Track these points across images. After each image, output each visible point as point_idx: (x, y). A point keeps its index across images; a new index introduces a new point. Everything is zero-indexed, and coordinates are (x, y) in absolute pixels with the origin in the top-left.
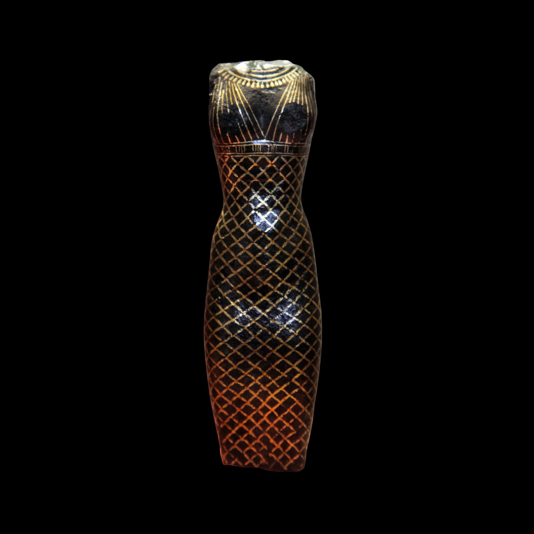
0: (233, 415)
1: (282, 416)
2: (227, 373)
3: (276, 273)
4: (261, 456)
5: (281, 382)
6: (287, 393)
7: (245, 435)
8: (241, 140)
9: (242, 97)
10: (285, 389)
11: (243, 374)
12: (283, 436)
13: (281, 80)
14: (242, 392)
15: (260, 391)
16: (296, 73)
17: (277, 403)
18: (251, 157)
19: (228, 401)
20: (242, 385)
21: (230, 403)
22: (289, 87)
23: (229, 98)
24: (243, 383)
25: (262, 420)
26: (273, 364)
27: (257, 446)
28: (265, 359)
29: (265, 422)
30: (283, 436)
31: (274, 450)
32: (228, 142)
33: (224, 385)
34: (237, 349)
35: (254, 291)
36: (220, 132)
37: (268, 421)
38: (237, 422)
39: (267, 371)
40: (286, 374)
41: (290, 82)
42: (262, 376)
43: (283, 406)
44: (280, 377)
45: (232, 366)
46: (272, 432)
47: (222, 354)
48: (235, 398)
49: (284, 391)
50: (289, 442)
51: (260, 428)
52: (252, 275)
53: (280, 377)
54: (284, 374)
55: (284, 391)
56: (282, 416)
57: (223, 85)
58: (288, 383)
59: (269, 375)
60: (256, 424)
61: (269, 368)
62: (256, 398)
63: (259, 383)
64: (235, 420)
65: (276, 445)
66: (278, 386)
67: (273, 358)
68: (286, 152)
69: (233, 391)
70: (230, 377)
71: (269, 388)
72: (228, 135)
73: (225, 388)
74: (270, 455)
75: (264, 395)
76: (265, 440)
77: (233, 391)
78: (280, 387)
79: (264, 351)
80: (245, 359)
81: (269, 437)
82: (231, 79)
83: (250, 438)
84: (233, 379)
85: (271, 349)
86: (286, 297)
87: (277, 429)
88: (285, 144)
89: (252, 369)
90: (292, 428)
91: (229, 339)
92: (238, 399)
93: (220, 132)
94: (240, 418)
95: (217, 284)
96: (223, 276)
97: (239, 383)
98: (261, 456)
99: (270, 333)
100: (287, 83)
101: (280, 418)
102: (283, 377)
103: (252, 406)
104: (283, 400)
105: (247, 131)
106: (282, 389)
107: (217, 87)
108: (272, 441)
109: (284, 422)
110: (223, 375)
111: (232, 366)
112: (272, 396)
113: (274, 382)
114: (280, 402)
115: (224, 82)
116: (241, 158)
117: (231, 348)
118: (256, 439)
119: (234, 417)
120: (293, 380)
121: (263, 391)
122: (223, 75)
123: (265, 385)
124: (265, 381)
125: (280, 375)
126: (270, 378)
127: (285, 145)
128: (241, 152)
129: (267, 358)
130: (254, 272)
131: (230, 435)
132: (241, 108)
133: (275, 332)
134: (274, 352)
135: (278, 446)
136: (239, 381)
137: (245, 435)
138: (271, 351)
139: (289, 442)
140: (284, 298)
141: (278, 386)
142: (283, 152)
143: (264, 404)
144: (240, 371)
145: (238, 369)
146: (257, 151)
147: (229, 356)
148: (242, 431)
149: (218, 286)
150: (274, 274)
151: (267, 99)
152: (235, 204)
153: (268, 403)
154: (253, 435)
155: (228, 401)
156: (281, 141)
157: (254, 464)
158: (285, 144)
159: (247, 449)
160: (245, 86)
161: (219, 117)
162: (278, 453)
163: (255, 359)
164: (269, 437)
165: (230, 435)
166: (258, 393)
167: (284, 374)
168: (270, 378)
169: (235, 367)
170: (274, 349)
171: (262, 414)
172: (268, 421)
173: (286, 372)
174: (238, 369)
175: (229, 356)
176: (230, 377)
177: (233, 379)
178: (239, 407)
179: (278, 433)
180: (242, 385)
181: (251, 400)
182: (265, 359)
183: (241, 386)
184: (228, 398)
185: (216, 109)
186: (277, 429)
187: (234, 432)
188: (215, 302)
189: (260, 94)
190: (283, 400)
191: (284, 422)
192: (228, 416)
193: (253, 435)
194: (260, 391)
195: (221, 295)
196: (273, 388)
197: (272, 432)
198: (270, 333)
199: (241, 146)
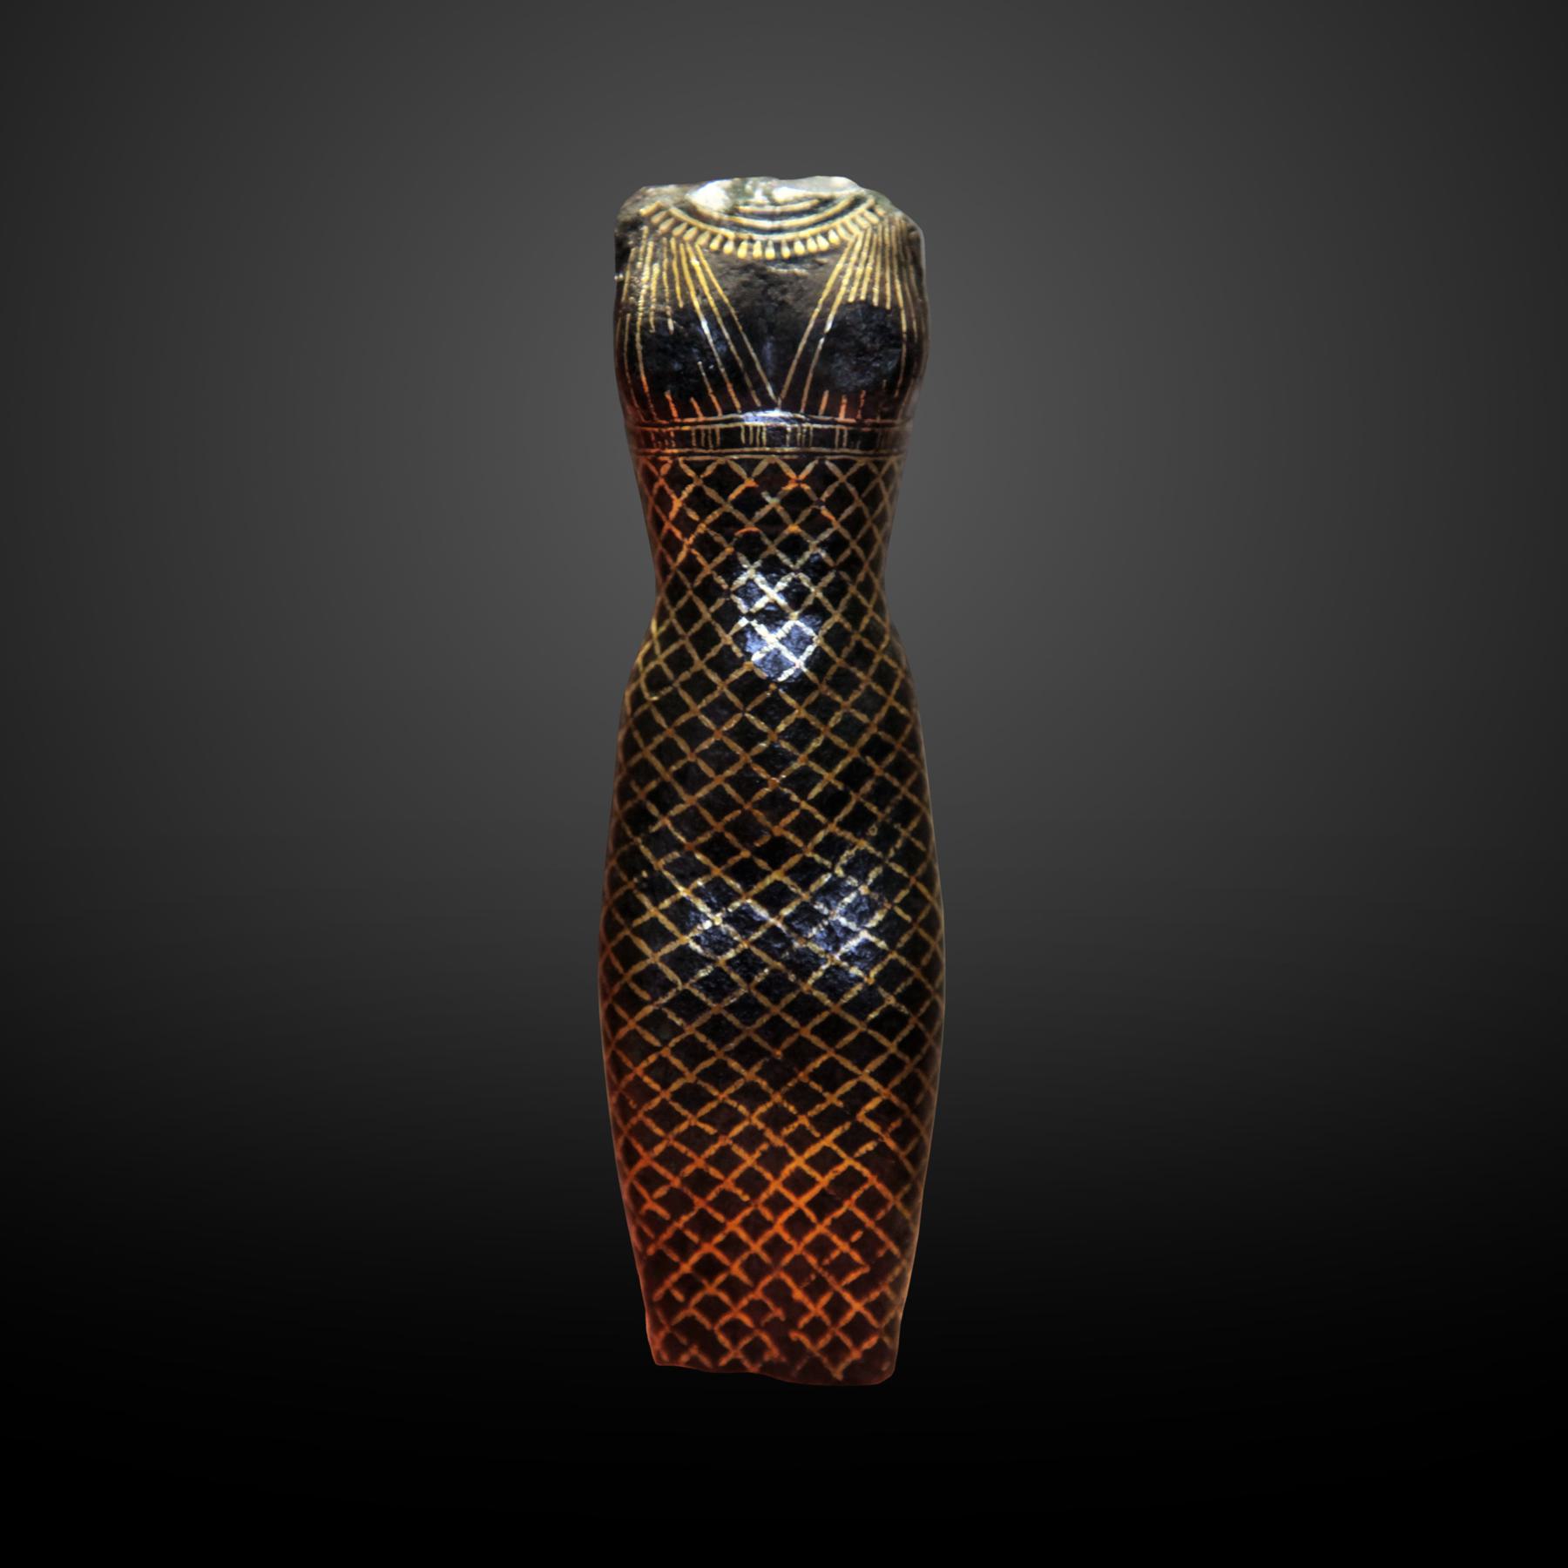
0: (685, 1218)
1: (828, 1221)
2: (666, 1095)
3: (811, 803)
4: (765, 1338)
5: (826, 1122)
6: (842, 1154)
7: (721, 1278)
8: (709, 410)
9: (710, 284)
10: (836, 1141)
11: (712, 1098)
12: (831, 1279)
13: (825, 234)
14: (712, 1151)
15: (764, 1147)
16: (868, 214)
17: (813, 1182)
18: (738, 462)
19: (669, 1176)
20: (710, 1130)
21: (676, 1183)
22: (849, 256)
23: (672, 287)
24: (713, 1124)
25: (769, 1234)
26: (802, 1068)
27: (756, 1309)
28: (779, 1053)
29: (777, 1238)
30: (831, 1279)
31: (804, 1321)
32: (668, 416)
33: (659, 1132)
34: (695, 1025)
35: (745, 854)
36: (646, 389)
37: (786, 1237)
38: (695, 1238)
39: (784, 1089)
40: (841, 1098)
41: (851, 240)
42: (769, 1105)
43: (832, 1193)
44: (821, 1107)
45: (680, 1074)
46: (798, 1269)
47: (651, 1039)
48: (689, 1170)
49: (835, 1147)
50: (847, 1297)
51: (765, 1257)
52: (740, 807)
53: (821, 1107)
54: (833, 1099)
55: (835, 1147)
56: (828, 1221)
57: (655, 250)
58: (847, 1126)
59: (789, 1102)
60: (751, 1244)
61: (789, 1079)
62: (750, 1169)
63: (761, 1126)
64: (689, 1234)
65: (810, 1306)
66: (817, 1135)
67: (803, 1053)
68: (840, 446)
69: (683, 1149)
70: (677, 1106)
71: (789, 1139)
72: (668, 396)
73: (660, 1139)
74: (794, 1335)
75: (775, 1159)
76: (779, 1292)
77: (683, 1149)
78: (822, 1137)
79: (776, 1030)
80: (720, 1055)
81: (790, 1282)
82: (677, 231)
83: (733, 1287)
84: (684, 1112)
85: (795, 1024)
86: (840, 872)
87: (812, 1260)
88: (836, 423)
89: (740, 1084)
90: (856, 1257)
91: (671, 995)
92: (698, 1171)
93: (646, 389)
94: (706, 1226)
95: (636, 833)
96: (654, 811)
97: (701, 1125)
98: (765, 1338)
99: (792, 977)
100: (843, 243)
101: (821, 1229)
102: (832, 1107)
103: (739, 1192)
104: (831, 1176)
105: (725, 385)
106: (828, 1141)
107: (637, 254)
108: (798, 1295)
109: (835, 1239)
110: (656, 1101)
111: (680, 1074)
112: (799, 1162)
113: (803, 1120)
114: (823, 1181)
115: (657, 241)
116: (709, 463)
117: (679, 1022)
118: (752, 1289)
119: (686, 1225)
120: (861, 1116)
121: (773, 1148)
122: (656, 219)
123: (777, 1132)
124: (777, 1119)
125: (823, 1100)
126: (792, 1109)
127: (838, 427)
128: (707, 447)
129: (784, 1052)
130: (747, 798)
131: (674, 1277)
132: (707, 318)
133: (808, 975)
134: (806, 1032)
135: (817, 1309)
136: (702, 1119)
137: (721, 1278)
138: (795, 1030)
139: (847, 1297)
140: (835, 875)
141: (817, 1135)
142: (832, 446)
143: (776, 1186)
144: (704, 1090)
145: (700, 1082)
146: (754, 445)
147: (672, 1044)
148: (709, 1267)
149: (639, 840)
150: (804, 805)
151: (784, 292)
152: (690, 599)
153: (786, 1184)
154: (744, 1278)
155: (669, 1176)
156: (826, 414)
157: (746, 1363)
158: (836, 423)
159: (726, 1318)
161: (643, 342)
162: (815, 1329)
163: (748, 1054)
164: (790, 1282)
165: (674, 1277)
166: (757, 1155)
167: (833, 1099)
168: (792, 1109)
169: (690, 1077)
170: (804, 1024)
171: (768, 1215)
172: (786, 1237)
173: (840, 1091)
174: (700, 1082)
175: (672, 1044)
176: (677, 1106)
177: (684, 1112)
178: (703, 1196)
179: (815, 1271)
180: (710, 1130)
181: (736, 1174)
182: (779, 1053)
183: (707, 1135)
184: (668, 1168)
185: (634, 320)
186: (812, 1260)
187: (686, 1268)
188: (631, 885)
189: (764, 277)
190: (831, 1176)
191: (835, 1239)
192: (670, 1223)
193: (744, 1278)
194: (764, 1147)
195: (649, 867)
196: (801, 1141)
197: (798, 1269)
198: (792, 977)
199: (709, 427)
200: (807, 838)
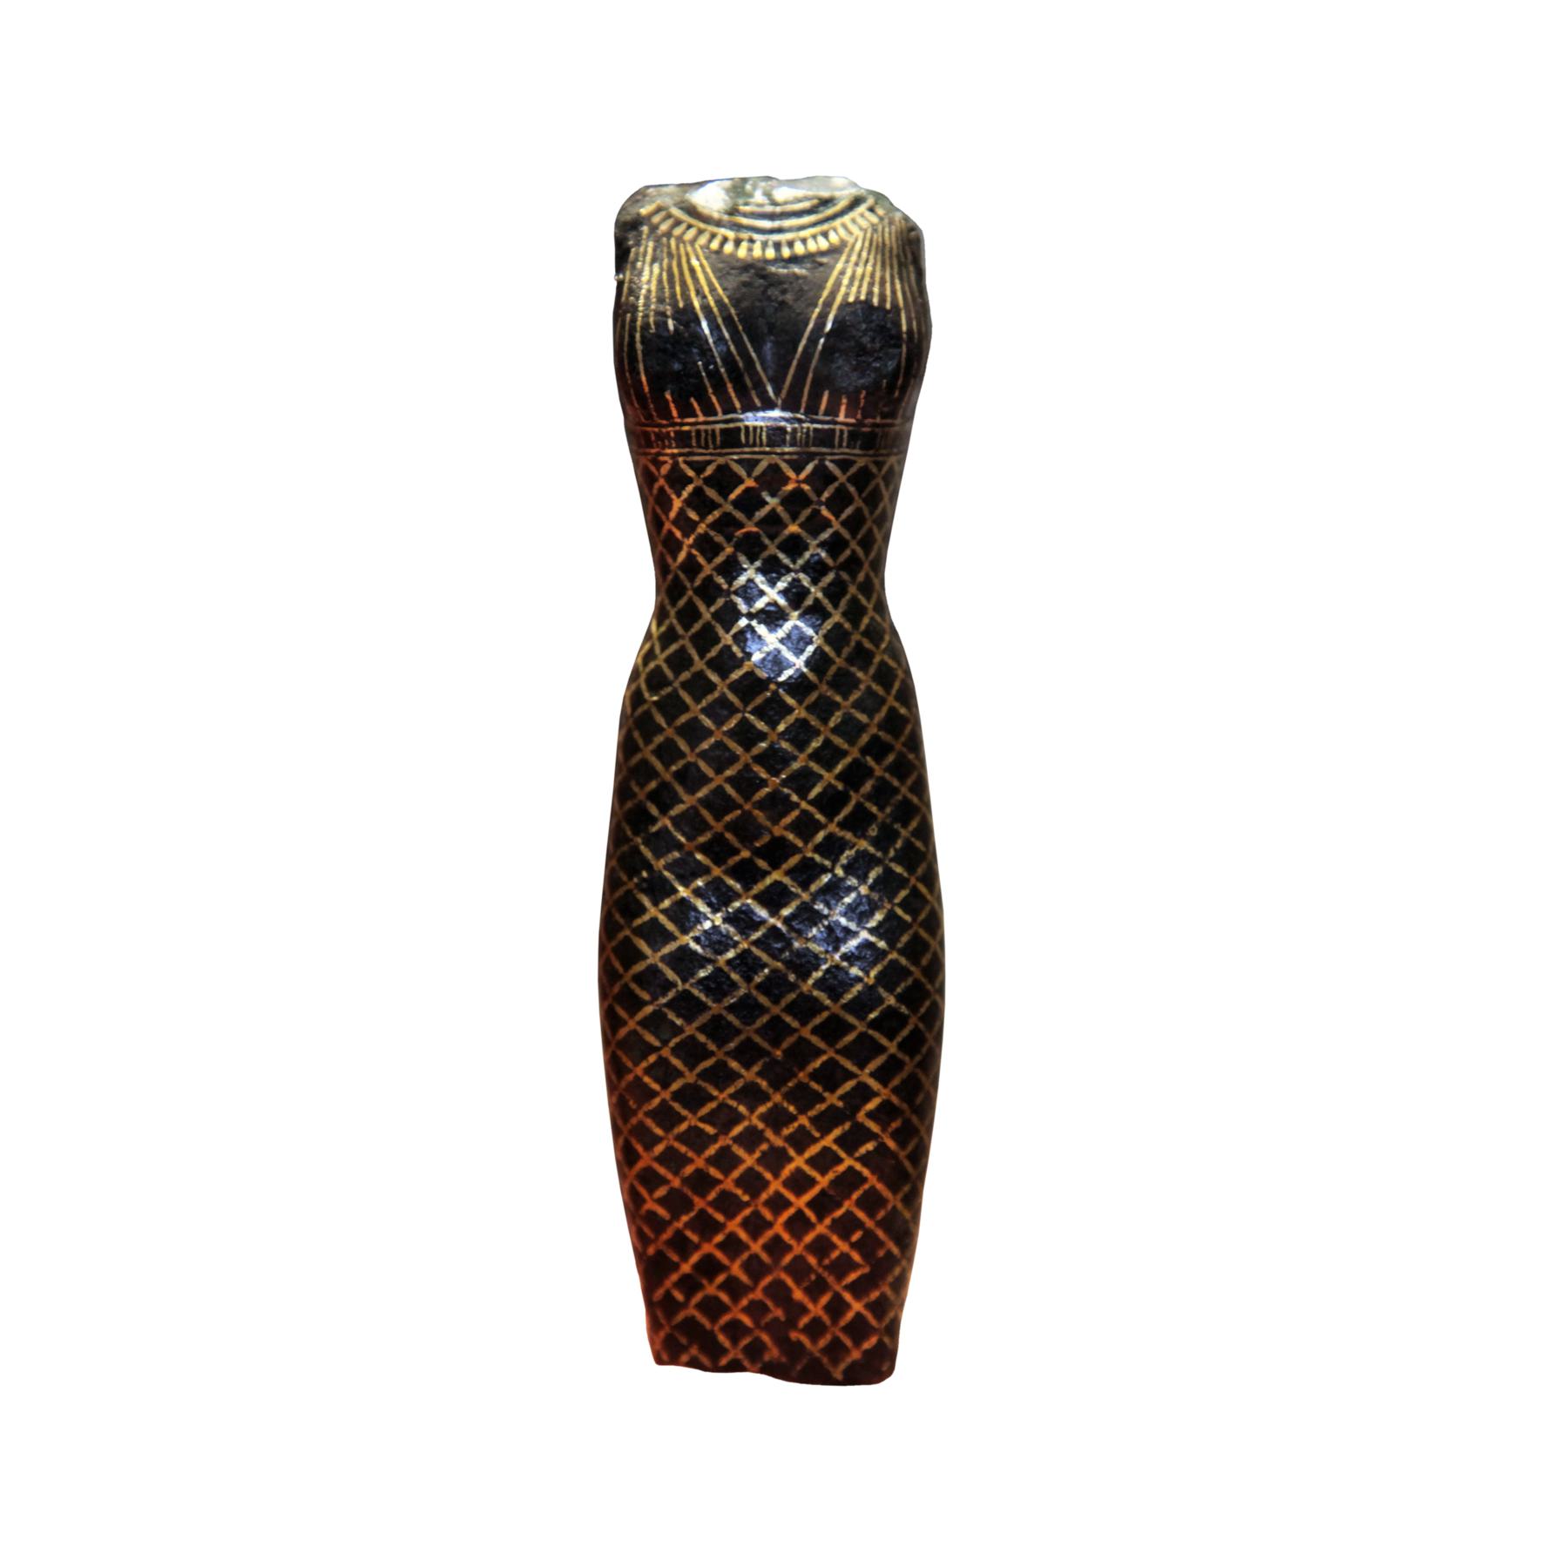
0: (685, 1218)
1: (828, 1221)
2: (666, 1095)
3: (811, 803)
4: (765, 1338)
5: (826, 1122)
6: (842, 1154)
7: (721, 1278)
8: (709, 410)
9: (710, 284)
10: (836, 1141)
11: (712, 1098)
12: (831, 1279)
13: (825, 234)
14: (712, 1151)
15: (764, 1147)
16: (868, 214)
17: (813, 1182)
18: (738, 462)
19: (669, 1176)
20: (710, 1130)
21: (676, 1183)
22: (849, 256)
23: (672, 287)
24: (713, 1124)
25: (769, 1234)
26: (802, 1068)
27: (756, 1309)
28: (779, 1053)
29: (777, 1238)
30: (831, 1279)
31: (804, 1321)
32: (668, 416)
33: (659, 1132)
34: (695, 1025)
35: (745, 854)
36: (646, 389)
37: (786, 1237)
38: (695, 1238)
39: (784, 1089)
40: (841, 1098)
41: (851, 240)
42: (769, 1105)
43: (832, 1193)
44: (821, 1107)
45: (680, 1074)
46: (798, 1269)
47: (651, 1039)
48: (689, 1170)
49: (835, 1147)
50: (847, 1297)
51: (765, 1257)
52: (740, 807)
53: (821, 1107)
54: (833, 1099)
55: (835, 1147)
56: (828, 1221)
57: (655, 250)
58: (847, 1126)
59: (789, 1102)
60: (751, 1244)
61: (789, 1079)
62: (750, 1169)
63: (761, 1126)
64: (689, 1234)
65: (810, 1306)
66: (817, 1135)
67: (803, 1053)
68: (840, 446)
69: (683, 1149)
70: (677, 1106)
71: (789, 1139)
72: (668, 396)
73: (660, 1139)
74: (794, 1335)
75: (775, 1159)
76: (779, 1292)
77: (683, 1149)
78: (822, 1137)
79: (776, 1030)
80: (720, 1055)
81: (790, 1282)
82: (677, 231)
83: (733, 1287)
84: (684, 1112)
85: (795, 1024)
86: (840, 872)
87: (812, 1260)
88: (836, 423)
89: (740, 1084)
90: (856, 1257)
91: (671, 995)
92: (698, 1171)
93: (646, 389)
94: (706, 1226)
95: (636, 833)
96: (654, 811)
97: (701, 1125)
98: (765, 1338)
99: (792, 977)
100: (843, 243)
101: (821, 1229)
102: (832, 1107)
103: (739, 1192)
104: (831, 1176)
105: (725, 385)
106: (828, 1141)
107: (637, 254)
108: (798, 1295)
109: (835, 1239)
110: (656, 1101)
111: (680, 1074)
112: (799, 1162)
113: (803, 1120)
114: (823, 1181)
115: (657, 241)
116: (709, 463)
117: (679, 1022)
118: (752, 1289)
119: (686, 1225)
120: (861, 1116)
121: (773, 1148)
123: (777, 1132)
124: (777, 1119)
125: (823, 1100)
126: (792, 1109)
127: (838, 427)
128: (707, 447)
129: (784, 1052)
130: (747, 798)
131: (674, 1277)
133: (808, 975)
134: (806, 1032)
135: (817, 1309)
136: (702, 1119)
137: (721, 1278)
138: (795, 1030)
139: (847, 1297)
140: (835, 875)
141: (817, 1135)
142: (832, 446)
143: (776, 1186)
144: (704, 1090)
145: (700, 1082)
146: (754, 445)
147: (672, 1044)
148: (709, 1267)
149: (639, 840)
150: (804, 805)
151: (784, 292)
152: (690, 599)
153: (786, 1184)
154: (744, 1278)
155: (669, 1176)
156: (826, 414)
158: (836, 423)
159: (726, 1318)
160: (719, 252)
161: (643, 342)
162: (815, 1329)
163: (748, 1054)
164: (790, 1282)
165: (674, 1277)
166: (757, 1155)
167: (833, 1099)
168: (792, 1109)
169: (690, 1077)
170: (804, 1024)
171: (768, 1215)
172: (786, 1237)
173: (840, 1091)
174: (700, 1082)
175: (672, 1044)
176: (677, 1106)
177: (684, 1112)
178: (703, 1196)
179: (815, 1271)
180: (710, 1130)
181: (736, 1174)
182: (779, 1053)
183: (707, 1135)
184: (668, 1168)
185: (634, 320)
186: (812, 1260)
187: (686, 1268)
188: (631, 885)
190: (831, 1176)
191: (835, 1239)
192: (670, 1223)
193: (744, 1278)
194: (764, 1147)
195: (649, 867)
196: (801, 1141)
197: (798, 1269)
198: (792, 977)
199: (709, 427)
200: (807, 838)
